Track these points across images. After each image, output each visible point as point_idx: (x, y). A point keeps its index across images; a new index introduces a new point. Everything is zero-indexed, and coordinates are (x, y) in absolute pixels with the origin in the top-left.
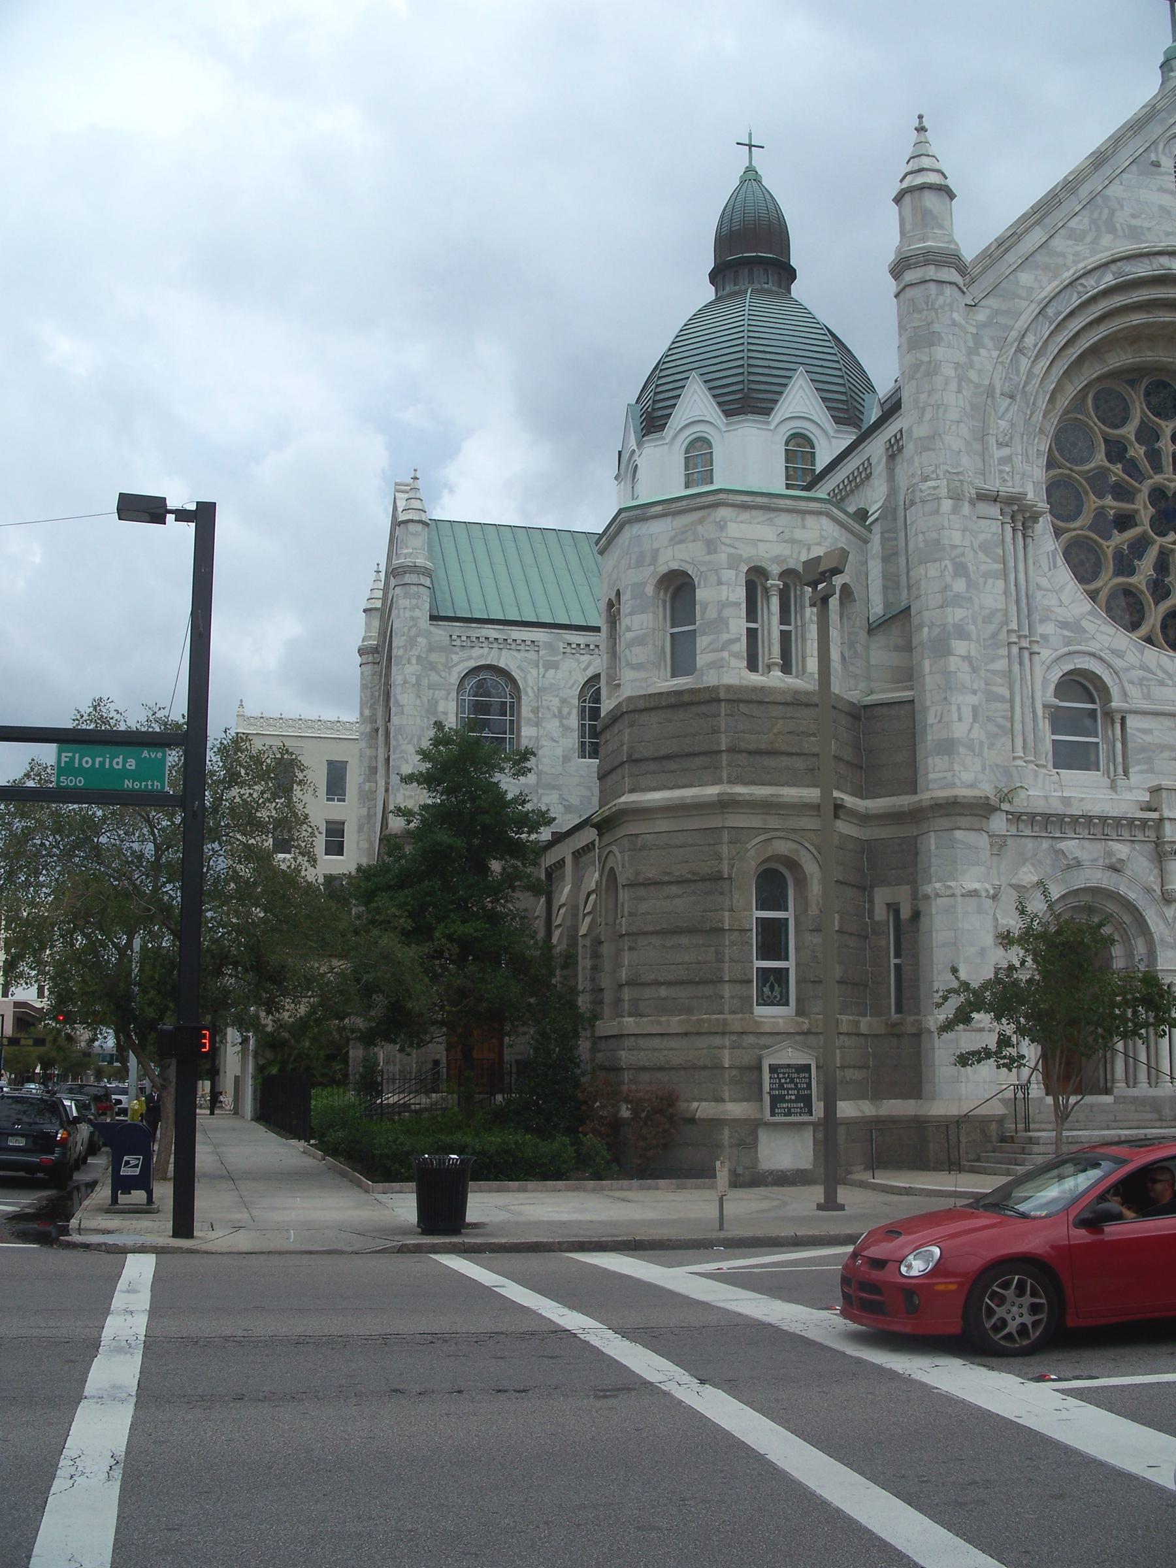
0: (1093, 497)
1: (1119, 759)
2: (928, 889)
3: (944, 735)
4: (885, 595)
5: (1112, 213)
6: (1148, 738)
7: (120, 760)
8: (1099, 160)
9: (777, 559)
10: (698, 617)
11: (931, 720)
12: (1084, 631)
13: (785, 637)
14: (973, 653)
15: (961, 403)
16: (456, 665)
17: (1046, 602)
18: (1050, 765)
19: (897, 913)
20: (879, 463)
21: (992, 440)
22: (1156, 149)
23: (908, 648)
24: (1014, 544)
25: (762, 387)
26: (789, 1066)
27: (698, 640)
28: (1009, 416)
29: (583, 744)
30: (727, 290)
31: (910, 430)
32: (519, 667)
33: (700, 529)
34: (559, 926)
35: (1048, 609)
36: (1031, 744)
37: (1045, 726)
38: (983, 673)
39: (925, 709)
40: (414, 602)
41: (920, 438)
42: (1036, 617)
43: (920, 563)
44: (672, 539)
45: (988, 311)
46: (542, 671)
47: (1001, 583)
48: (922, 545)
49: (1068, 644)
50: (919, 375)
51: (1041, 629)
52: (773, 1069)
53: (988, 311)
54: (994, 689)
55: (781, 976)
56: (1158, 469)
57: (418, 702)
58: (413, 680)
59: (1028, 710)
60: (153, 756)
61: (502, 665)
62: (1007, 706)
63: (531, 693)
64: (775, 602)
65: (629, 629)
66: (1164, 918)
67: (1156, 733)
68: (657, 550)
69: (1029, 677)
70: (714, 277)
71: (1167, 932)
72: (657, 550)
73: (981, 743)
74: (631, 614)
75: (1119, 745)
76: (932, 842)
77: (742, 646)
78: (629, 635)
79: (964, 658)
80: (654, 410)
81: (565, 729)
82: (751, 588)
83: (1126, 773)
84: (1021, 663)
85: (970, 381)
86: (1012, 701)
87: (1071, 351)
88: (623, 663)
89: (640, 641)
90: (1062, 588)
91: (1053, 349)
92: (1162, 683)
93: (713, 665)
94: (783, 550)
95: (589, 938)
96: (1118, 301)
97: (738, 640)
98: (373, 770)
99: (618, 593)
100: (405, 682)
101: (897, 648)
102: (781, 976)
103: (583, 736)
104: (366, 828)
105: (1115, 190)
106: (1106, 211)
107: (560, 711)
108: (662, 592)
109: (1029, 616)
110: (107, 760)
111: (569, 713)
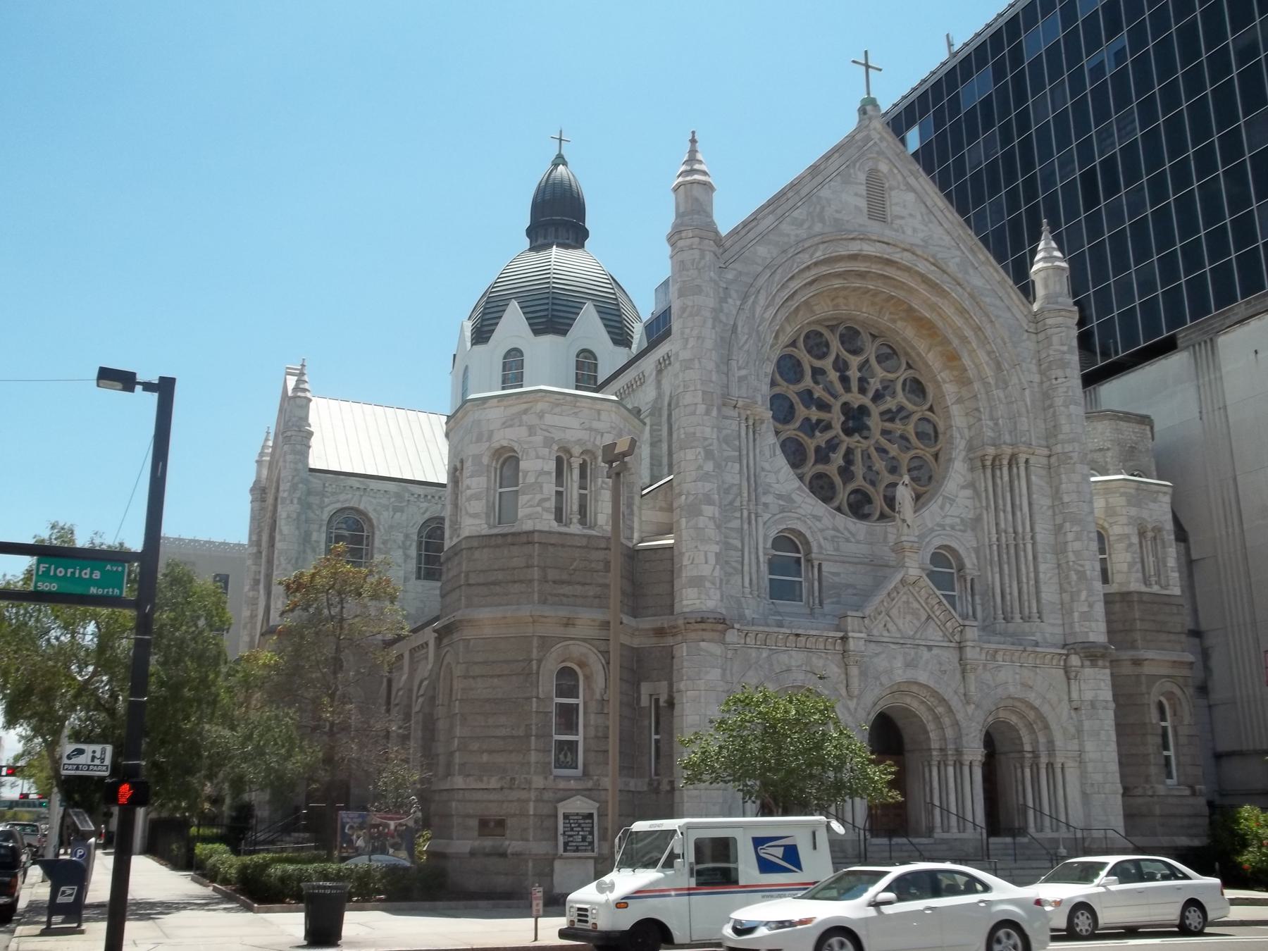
0: (802, 408)
1: (816, 594)
2: (682, 686)
3: (695, 573)
4: (652, 470)
5: (823, 208)
6: (837, 579)
7: (88, 571)
8: (814, 170)
9: (579, 442)
10: (521, 482)
11: (685, 562)
12: (794, 502)
13: (583, 498)
14: (717, 515)
15: (714, 336)
16: (328, 505)
17: (768, 480)
18: (768, 597)
19: (657, 701)
20: (651, 374)
21: (734, 363)
22: (854, 166)
23: (670, 509)
24: (747, 438)
25: (561, 314)
26: (577, 814)
27: (520, 498)
28: (746, 347)
29: (419, 568)
30: (539, 242)
31: (677, 354)
32: (375, 510)
33: (525, 417)
34: (397, 705)
35: (769, 485)
36: (755, 581)
37: (764, 568)
38: (723, 530)
39: (682, 554)
40: (298, 457)
41: (684, 360)
42: (760, 490)
43: (681, 449)
44: (504, 424)
45: (735, 272)
46: (391, 513)
47: (737, 466)
48: (683, 436)
49: (782, 511)
50: (685, 315)
51: (764, 499)
52: (566, 817)
53: (735, 272)
54: (731, 541)
55: (572, 746)
56: (848, 389)
57: (297, 533)
58: (294, 516)
59: (753, 557)
60: (88, 571)
61: (362, 507)
62: (739, 553)
63: (383, 530)
64: (576, 473)
65: (468, 488)
66: (848, 709)
67: (842, 576)
68: (492, 431)
69: (754, 533)
70: (530, 232)
71: (850, 719)
72: (492, 431)
73: (721, 580)
74: (471, 476)
75: (816, 584)
76: (682, 651)
77: (551, 504)
78: (469, 492)
79: (710, 518)
80: (482, 326)
81: (407, 557)
82: (559, 461)
83: (821, 603)
84: (750, 523)
85: (721, 322)
86: (742, 551)
87: (790, 303)
88: (463, 512)
89: (476, 497)
90: (779, 471)
91: (779, 301)
92: (848, 540)
93: (529, 517)
94: (584, 435)
95: (421, 714)
96: (824, 270)
97: (548, 499)
98: (257, 582)
99: (462, 462)
100: (288, 517)
101: (661, 509)
102: (572, 746)
103: (420, 563)
104: (249, 626)
105: (825, 193)
106: (818, 208)
107: (403, 542)
108: (494, 462)
109: (756, 490)
110: (77, 572)
111: (410, 545)
